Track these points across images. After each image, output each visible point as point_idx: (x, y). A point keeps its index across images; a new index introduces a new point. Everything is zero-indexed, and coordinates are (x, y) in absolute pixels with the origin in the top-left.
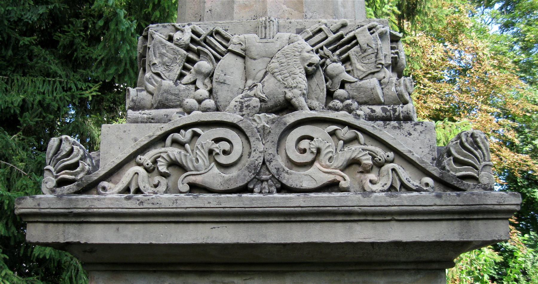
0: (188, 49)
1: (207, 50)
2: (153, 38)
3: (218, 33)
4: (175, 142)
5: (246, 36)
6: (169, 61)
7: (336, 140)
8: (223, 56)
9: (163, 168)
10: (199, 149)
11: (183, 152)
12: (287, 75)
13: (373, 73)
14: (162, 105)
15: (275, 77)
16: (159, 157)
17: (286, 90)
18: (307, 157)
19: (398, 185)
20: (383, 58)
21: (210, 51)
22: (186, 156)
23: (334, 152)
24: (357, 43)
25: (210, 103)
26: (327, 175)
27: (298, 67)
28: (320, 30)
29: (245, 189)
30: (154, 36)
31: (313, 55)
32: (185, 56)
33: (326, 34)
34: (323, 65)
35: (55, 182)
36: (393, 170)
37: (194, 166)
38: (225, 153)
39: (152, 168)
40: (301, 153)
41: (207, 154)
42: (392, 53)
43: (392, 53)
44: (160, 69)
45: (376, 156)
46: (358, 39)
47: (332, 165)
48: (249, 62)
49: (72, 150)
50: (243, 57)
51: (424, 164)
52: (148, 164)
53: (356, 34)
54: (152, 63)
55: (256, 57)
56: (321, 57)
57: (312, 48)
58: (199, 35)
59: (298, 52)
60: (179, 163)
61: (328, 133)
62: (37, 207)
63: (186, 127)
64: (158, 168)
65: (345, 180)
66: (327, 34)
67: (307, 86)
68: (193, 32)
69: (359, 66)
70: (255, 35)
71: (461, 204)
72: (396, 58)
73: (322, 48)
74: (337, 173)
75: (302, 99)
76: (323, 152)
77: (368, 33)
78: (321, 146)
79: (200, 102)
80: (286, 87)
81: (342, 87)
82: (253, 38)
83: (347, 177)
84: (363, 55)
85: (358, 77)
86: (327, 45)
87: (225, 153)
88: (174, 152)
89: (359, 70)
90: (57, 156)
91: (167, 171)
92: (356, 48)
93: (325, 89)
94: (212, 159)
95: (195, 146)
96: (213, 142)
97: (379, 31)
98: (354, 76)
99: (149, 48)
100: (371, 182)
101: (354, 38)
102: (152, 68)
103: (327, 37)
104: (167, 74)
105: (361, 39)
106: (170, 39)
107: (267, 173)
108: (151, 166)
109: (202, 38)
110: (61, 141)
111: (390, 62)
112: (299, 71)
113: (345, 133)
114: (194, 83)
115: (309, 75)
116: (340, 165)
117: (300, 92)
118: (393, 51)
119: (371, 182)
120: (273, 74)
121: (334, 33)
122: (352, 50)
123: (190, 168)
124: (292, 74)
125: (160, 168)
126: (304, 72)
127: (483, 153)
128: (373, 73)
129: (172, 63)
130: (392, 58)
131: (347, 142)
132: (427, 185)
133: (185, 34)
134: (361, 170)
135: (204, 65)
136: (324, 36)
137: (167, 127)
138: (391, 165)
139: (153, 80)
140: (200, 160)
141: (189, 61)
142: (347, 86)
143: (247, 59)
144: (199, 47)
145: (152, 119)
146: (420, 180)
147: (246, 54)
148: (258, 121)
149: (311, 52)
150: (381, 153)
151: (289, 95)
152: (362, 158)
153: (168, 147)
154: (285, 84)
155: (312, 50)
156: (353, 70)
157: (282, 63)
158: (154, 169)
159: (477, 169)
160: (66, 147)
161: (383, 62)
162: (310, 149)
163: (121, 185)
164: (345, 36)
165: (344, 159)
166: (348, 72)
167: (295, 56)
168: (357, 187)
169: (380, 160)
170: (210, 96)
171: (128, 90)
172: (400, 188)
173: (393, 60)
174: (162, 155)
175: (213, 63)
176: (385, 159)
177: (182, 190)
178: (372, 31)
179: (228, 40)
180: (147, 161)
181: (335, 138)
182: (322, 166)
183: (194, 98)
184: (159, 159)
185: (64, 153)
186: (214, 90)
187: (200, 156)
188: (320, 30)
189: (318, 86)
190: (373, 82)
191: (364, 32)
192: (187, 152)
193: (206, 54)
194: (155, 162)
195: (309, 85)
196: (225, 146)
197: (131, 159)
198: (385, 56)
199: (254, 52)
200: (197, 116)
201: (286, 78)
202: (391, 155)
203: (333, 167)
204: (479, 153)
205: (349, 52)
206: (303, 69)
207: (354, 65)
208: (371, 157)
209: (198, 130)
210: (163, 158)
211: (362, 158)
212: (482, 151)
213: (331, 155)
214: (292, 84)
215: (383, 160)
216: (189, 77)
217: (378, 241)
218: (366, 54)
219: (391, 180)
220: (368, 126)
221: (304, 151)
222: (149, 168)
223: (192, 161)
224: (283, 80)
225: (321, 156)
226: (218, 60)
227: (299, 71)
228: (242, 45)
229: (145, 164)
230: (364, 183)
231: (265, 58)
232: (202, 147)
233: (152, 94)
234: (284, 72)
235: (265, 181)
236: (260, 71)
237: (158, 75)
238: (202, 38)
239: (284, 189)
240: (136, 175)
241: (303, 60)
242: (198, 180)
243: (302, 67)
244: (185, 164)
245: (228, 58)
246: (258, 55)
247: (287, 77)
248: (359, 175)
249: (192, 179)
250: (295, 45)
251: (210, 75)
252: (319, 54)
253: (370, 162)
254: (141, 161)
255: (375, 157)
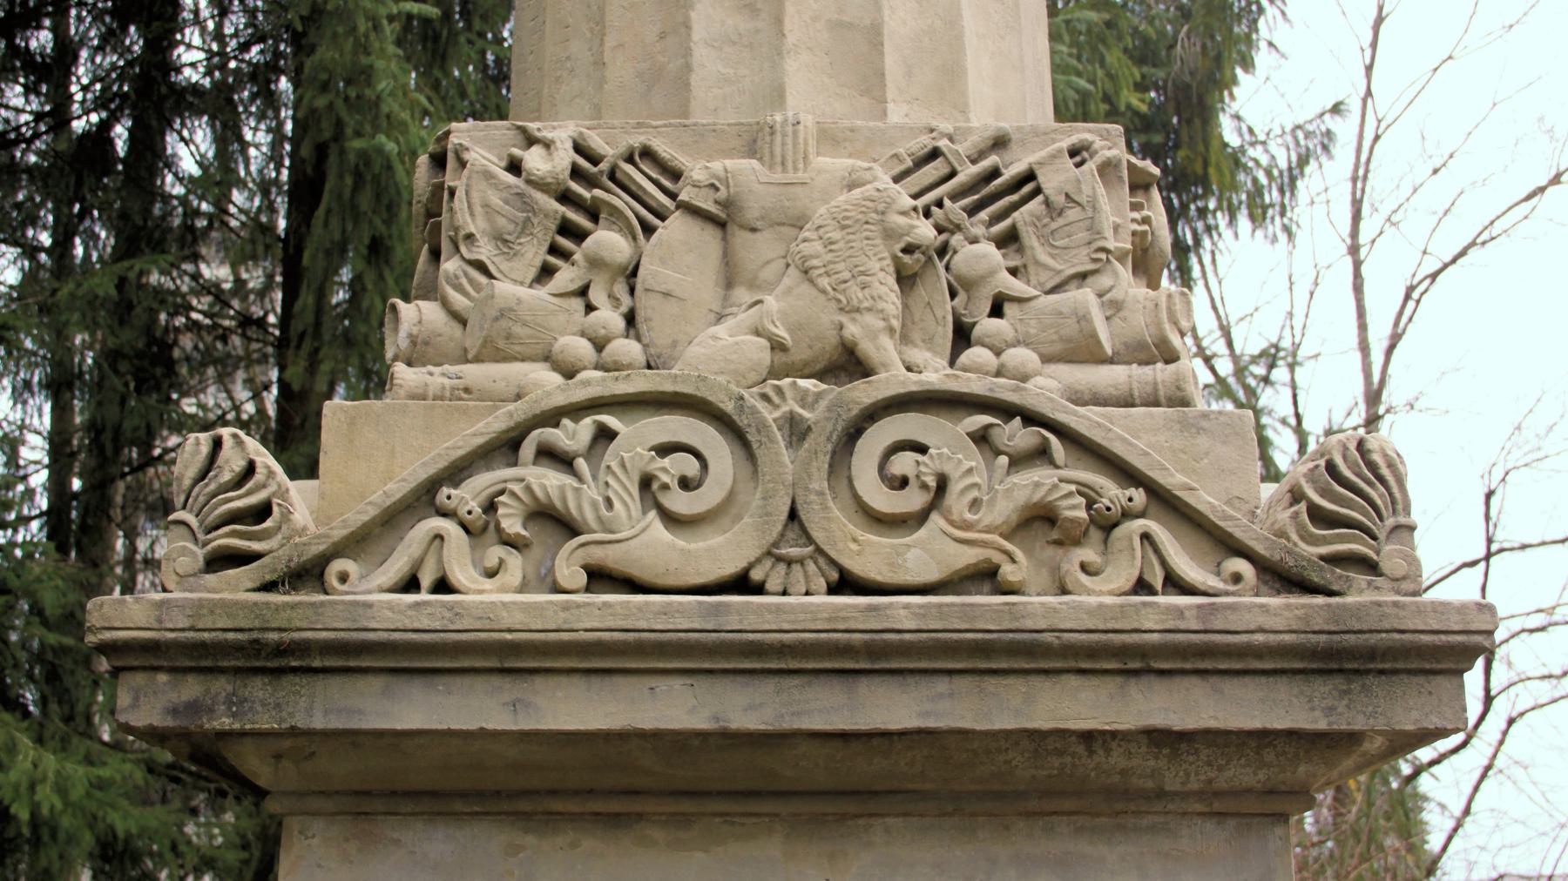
0: (565, 197)
1: (620, 201)
2: (463, 164)
3: (648, 153)
4: (551, 456)
5: (729, 163)
6: (511, 227)
7: (989, 454)
8: (663, 218)
9: (512, 524)
10: (614, 474)
11: (569, 480)
12: (847, 275)
13: (1083, 277)
14: (492, 352)
15: (811, 281)
16: (502, 492)
17: (844, 319)
18: (912, 500)
19: (1158, 581)
20: (1109, 233)
21: (626, 203)
22: (577, 490)
23: (985, 487)
24: (1038, 191)
25: (627, 349)
26: (965, 548)
27: (875, 255)
28: (935, 154)
29: (741, 584)
30: (466, 156)
31: (916, 222)
32: (559, 217)
33: (950, 163)
34: (942, 251)
35: (201, 559)
36: (1146, 537)
37: (600, 519)
38: (686, 484)
39: (480, 523)
40: (892, 488)
41: (637, 486)
42: (1133, 220)
43: (1133, 220)
44: (485, 251)
45: (1096, 497)
46: (1041, 178)
47: (978, 521)
48: (740, 238)
49: (251, 469)
50: (721, 225)
51: (1229, 523)
52: (470, 513)
53: (1035, 167)
54: (462, 233)
55: (759, 224)
56: (940, 230)
57: (913, 203)
58: (594, 160)
59: (876, 212)
60: (554, 507)
61: (968, 434)
62: (155, 625)
63: (577, 411)
64: (498, 525)
65: (1013, 561)
66: (956, 165)
67: (900, 307)
68: (579, 148)
69: (1042, 255)
70: (754, 162)
71: (1333, 628)
72: (1144, 233)
73: (940, 204)
74: (993, 542)
75: (888, 343)
76: (955, 488)
77: (1070, 163)
78: (947, 468)
79: (599, 346)
80: (841, 309)
81: (997, 311)
82: (745, 169)
83: (1019, 554)
84: (1054, 225)
85: (1041, 284)
86: (954, 197)
87: (686, 484)
88: (549, 481)
89: (1045, 267)
90: (207, 485)
91: (524, 533)
92: (1035, 205)
93: (950, 318)
94: (651, 503)
95: (603, 466)
96: (653, 453)
97: (1098, 159)
98: (1028, 283)
99: (452, 193)
100: (1084, 567)
101: (1030, 176)
102: (463, 249)
103: (953, 174)
104: (505, 266)
105: (1048, 179)
106: (515, 167)
107: (803, 540)
108: (480, 517)
109: (604, 166)
110: (217, 443)
111: (1129, 246)
112: (878, 266)
113: (1016, 435)
114: (583, 292)
115: (906, 280)
116: (999, 521)
117: (882, 324)
118: (1136, 215)
119: (1084, 567)
120: (806, 272)
121: (974, 162)
122: (1024, 209)
123: (587, 524)
124: (860, 275)
125: (505, 524)
126: (891, 269)
127: (1391, 494)
128: (1083, 277)
129: (522, 233)
130: (1134, 234)
131: (1019, 461)
132: (1237, 578)
133: (555, 154)
134: (1055, 535)
135: (608, 241)
136: (946, 170)
137: (518, 412)
138: (1139, 525)
139: (464, 281)
140: (617, 504)
141: (566, 229)
142: (1009, 309)
143: (731, 228)
144: (597, 192)
145: (467, 390)
146: (1219, 564)
147: (728, 215)
148: (776, 399)
149: (913, 213)
150: (1113, 493)
151: (852, 330)
152: (1059, 503)
153: (525, 465)
154: (839, 301)
155: (915, 209)
156: (1025, 266)
157: (832, 243)
158: (485, 528)
159: (1374, 538)
160: (232, 462)
161: (1111, 244)
162: (918, 477)
163: (396, 567)
164: (1003, 171)
165: (1011, 506)
166: (1014, 272)
167: (867, 223)
168: (1043, 578)
169: (1108, 509)
170: (627, 330)
171: (394, 308)
172: (1164, 585)
173: (1137, 240)
174: (510, 486)
175: (634, 238)
176: (1122, 507)
177: (564, 584)
178: (1078, 159)
179: (676, 175)
180: (467, 503)
181: (986, 448)
182: (952, 523)
183: (583, 334)
184: (501, 498)
185: (227, 476)
186: (639, 318)
187: (616, 493)
188: (935, 154)
189: (928, 310)
190: (1084, 296)
191: (1057, 161)
192: (580, 479)
193: (615, 211)
194: (490, 507)
195: (905, 306)
196: (686, 465)
197: (425, 499)
198: (1116, 228)
199: (752, 213)
200: (593, 383)
201: (843, 286)
202: (1139, 496)
203: (980, 527)
204: (1381, 496)
205: (1016, 215)
206: (888, 261)
207: (1028, 252)
208: (1083, 500)
209: (610, 420)
210: (513, 494)
211: (1059, 503)
212: (1387, 488)
213: (975, 493)
214: (860, 301)
215: (1116, 510)
216: (566, 277)
217: (1107, 728)
218: (1060, 222)
219: (1138, 563)
220: (1084, 420)
221: (903, 482)
222: (474, 522)
223: (594, 505)
224: (834, 289)
225: (947, 495)
226: (649, 230)
227: (878, 266)
228: (717, 189)
229: (462, 512)
230: (1067, 571)
231: (782, 229)
232: (623, 465)
233: (464, 323)
234: (841, 266)
235: (797, 562)
236: (768, 262)
237: (481, 267)
238: (604, 166)
239: (846, 583)
240: (437, 542)
241: (889, 234)
242: (610, 557)
243: (886, 254)
244: (574, 512)
245: (676, 228)
246: (763, 218)
247: (845, 282)
248: (1051, 551)
249: (598, 555)
250: (867, 194)
251: (631, 274)
252: (931, 220)
253: (1082, 514)
254: (452, 504)
255: (1095, 502)
